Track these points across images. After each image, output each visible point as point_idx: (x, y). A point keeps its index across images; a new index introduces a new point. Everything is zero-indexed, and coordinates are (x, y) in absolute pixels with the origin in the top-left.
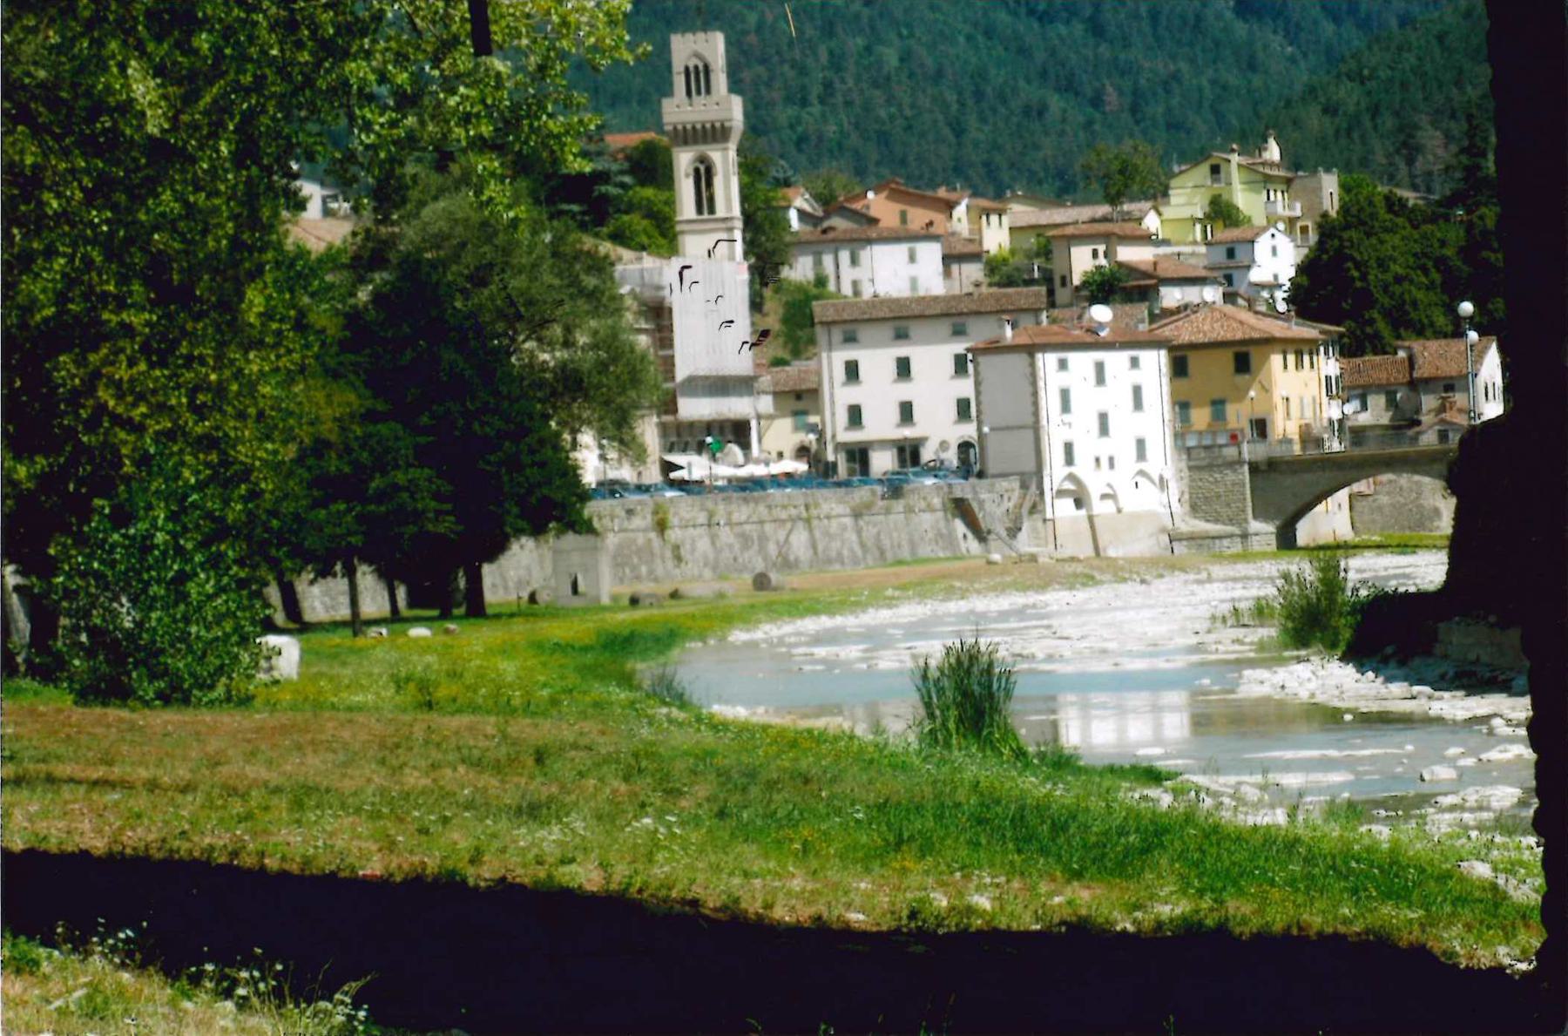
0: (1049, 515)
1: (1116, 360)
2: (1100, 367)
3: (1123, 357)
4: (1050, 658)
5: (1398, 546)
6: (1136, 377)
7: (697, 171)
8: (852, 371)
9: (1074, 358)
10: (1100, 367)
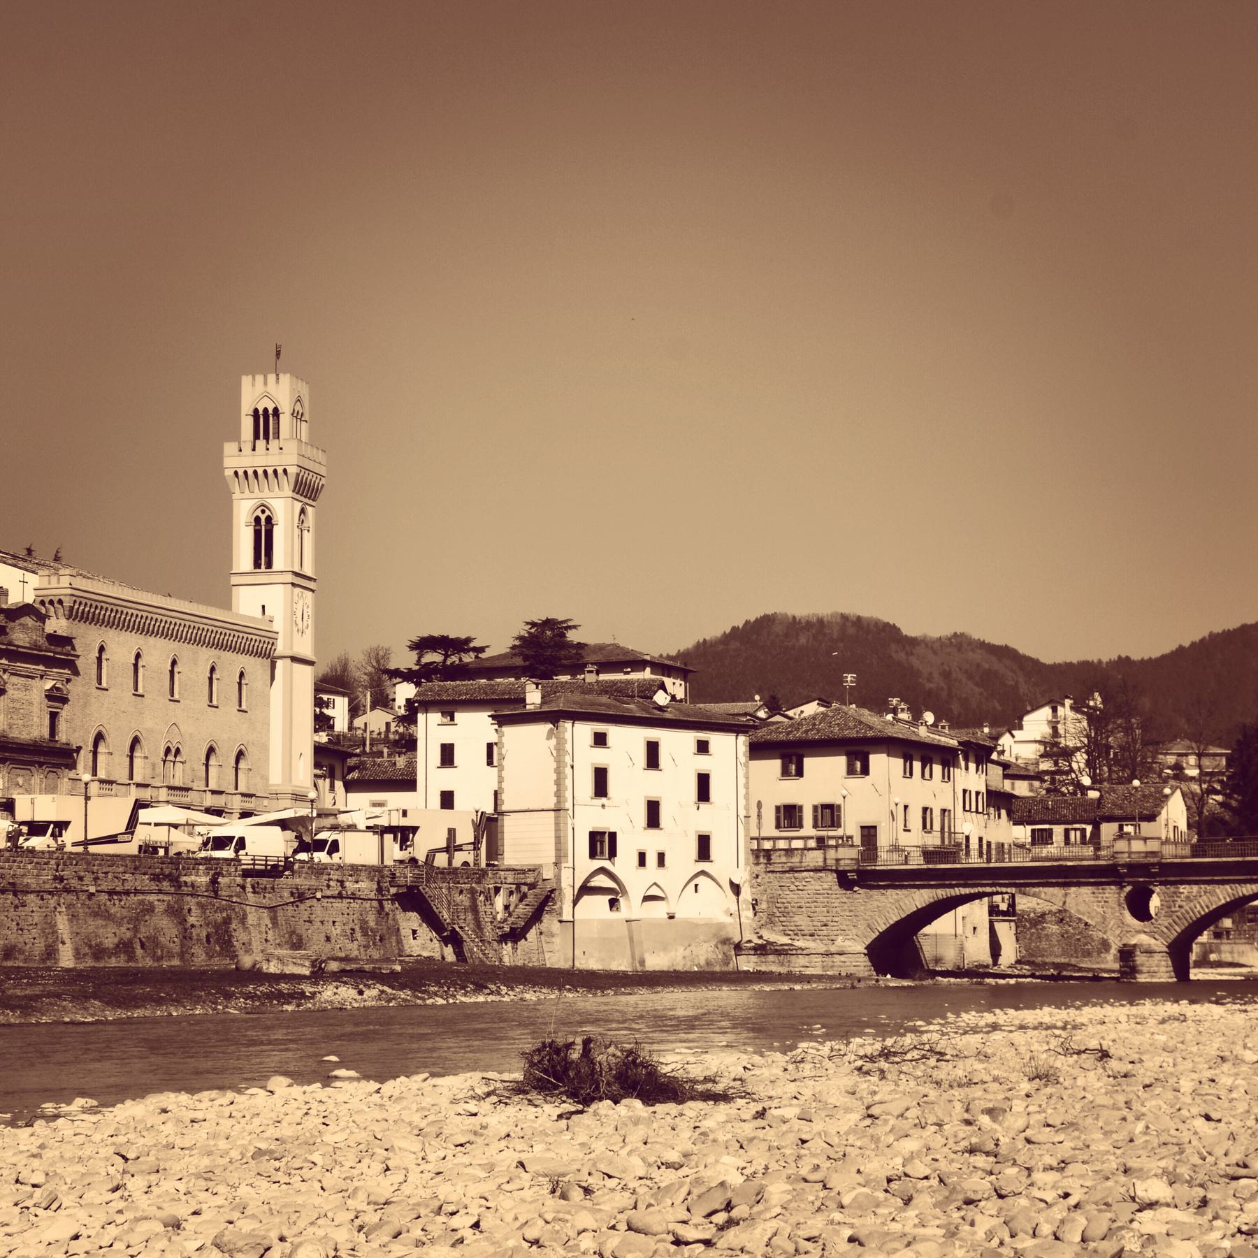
0: (567, 916)
1: (676, 743)
2: (653, 750)
3: (688, 738)
4: (673, 1071)
5: (202, 1073)
6: (704, 763)
7: (257, 520)
8: (447, 755)
9: (615, 733)
10: (653, 750)
